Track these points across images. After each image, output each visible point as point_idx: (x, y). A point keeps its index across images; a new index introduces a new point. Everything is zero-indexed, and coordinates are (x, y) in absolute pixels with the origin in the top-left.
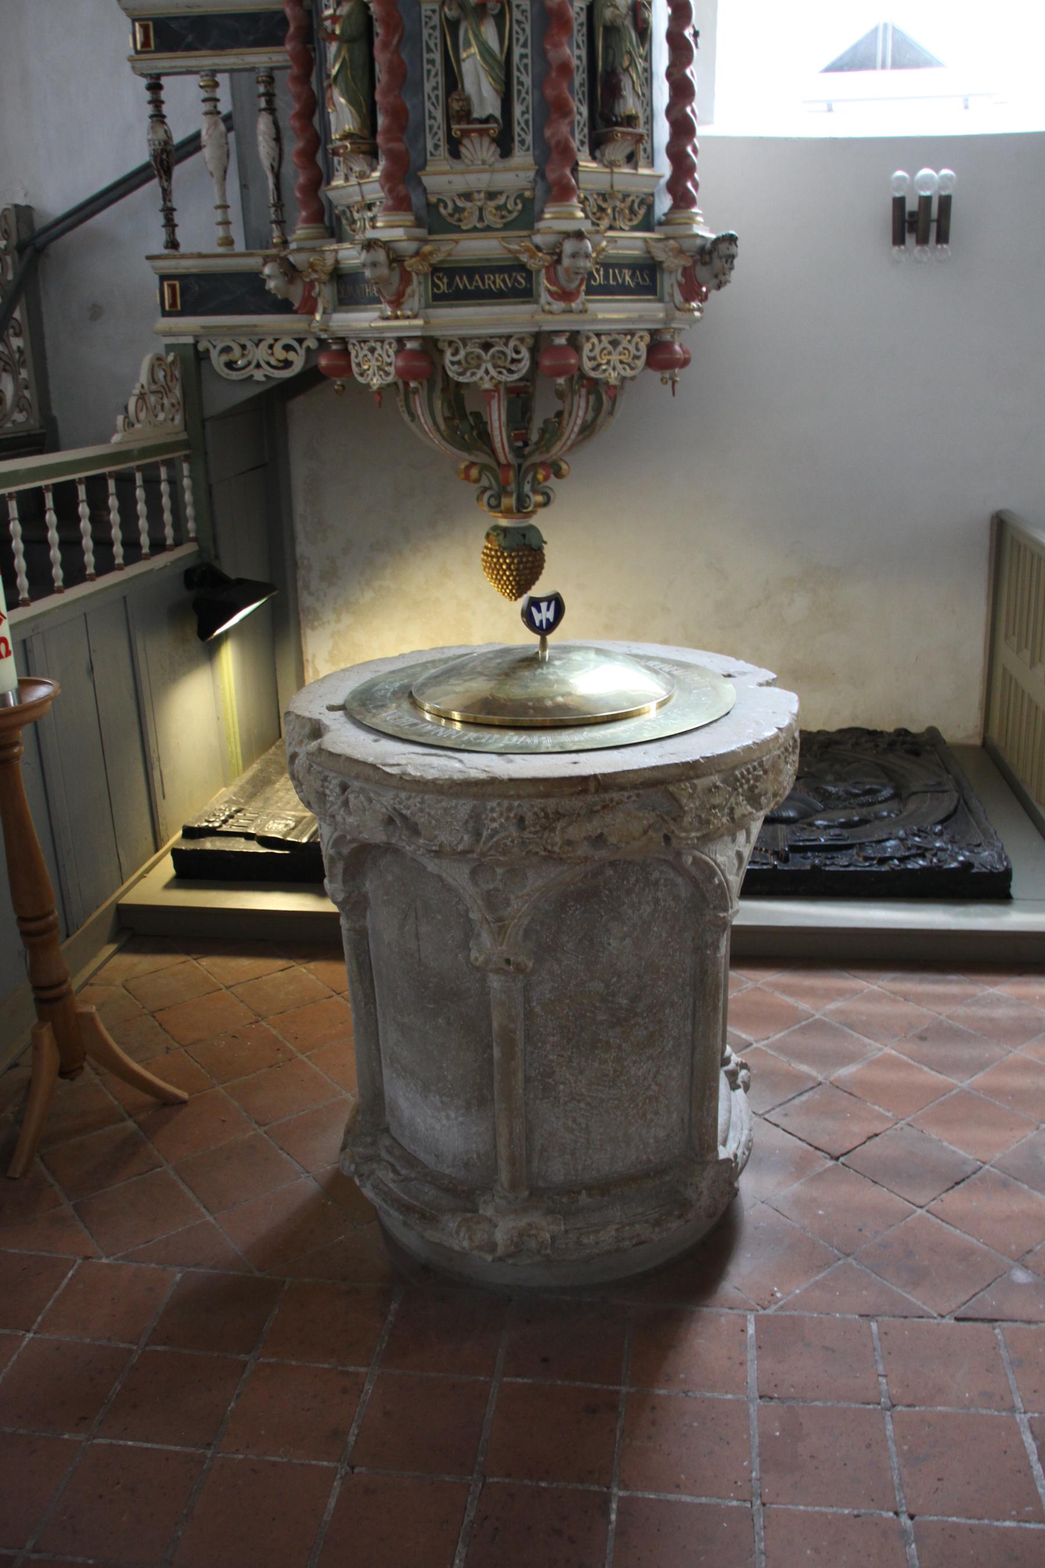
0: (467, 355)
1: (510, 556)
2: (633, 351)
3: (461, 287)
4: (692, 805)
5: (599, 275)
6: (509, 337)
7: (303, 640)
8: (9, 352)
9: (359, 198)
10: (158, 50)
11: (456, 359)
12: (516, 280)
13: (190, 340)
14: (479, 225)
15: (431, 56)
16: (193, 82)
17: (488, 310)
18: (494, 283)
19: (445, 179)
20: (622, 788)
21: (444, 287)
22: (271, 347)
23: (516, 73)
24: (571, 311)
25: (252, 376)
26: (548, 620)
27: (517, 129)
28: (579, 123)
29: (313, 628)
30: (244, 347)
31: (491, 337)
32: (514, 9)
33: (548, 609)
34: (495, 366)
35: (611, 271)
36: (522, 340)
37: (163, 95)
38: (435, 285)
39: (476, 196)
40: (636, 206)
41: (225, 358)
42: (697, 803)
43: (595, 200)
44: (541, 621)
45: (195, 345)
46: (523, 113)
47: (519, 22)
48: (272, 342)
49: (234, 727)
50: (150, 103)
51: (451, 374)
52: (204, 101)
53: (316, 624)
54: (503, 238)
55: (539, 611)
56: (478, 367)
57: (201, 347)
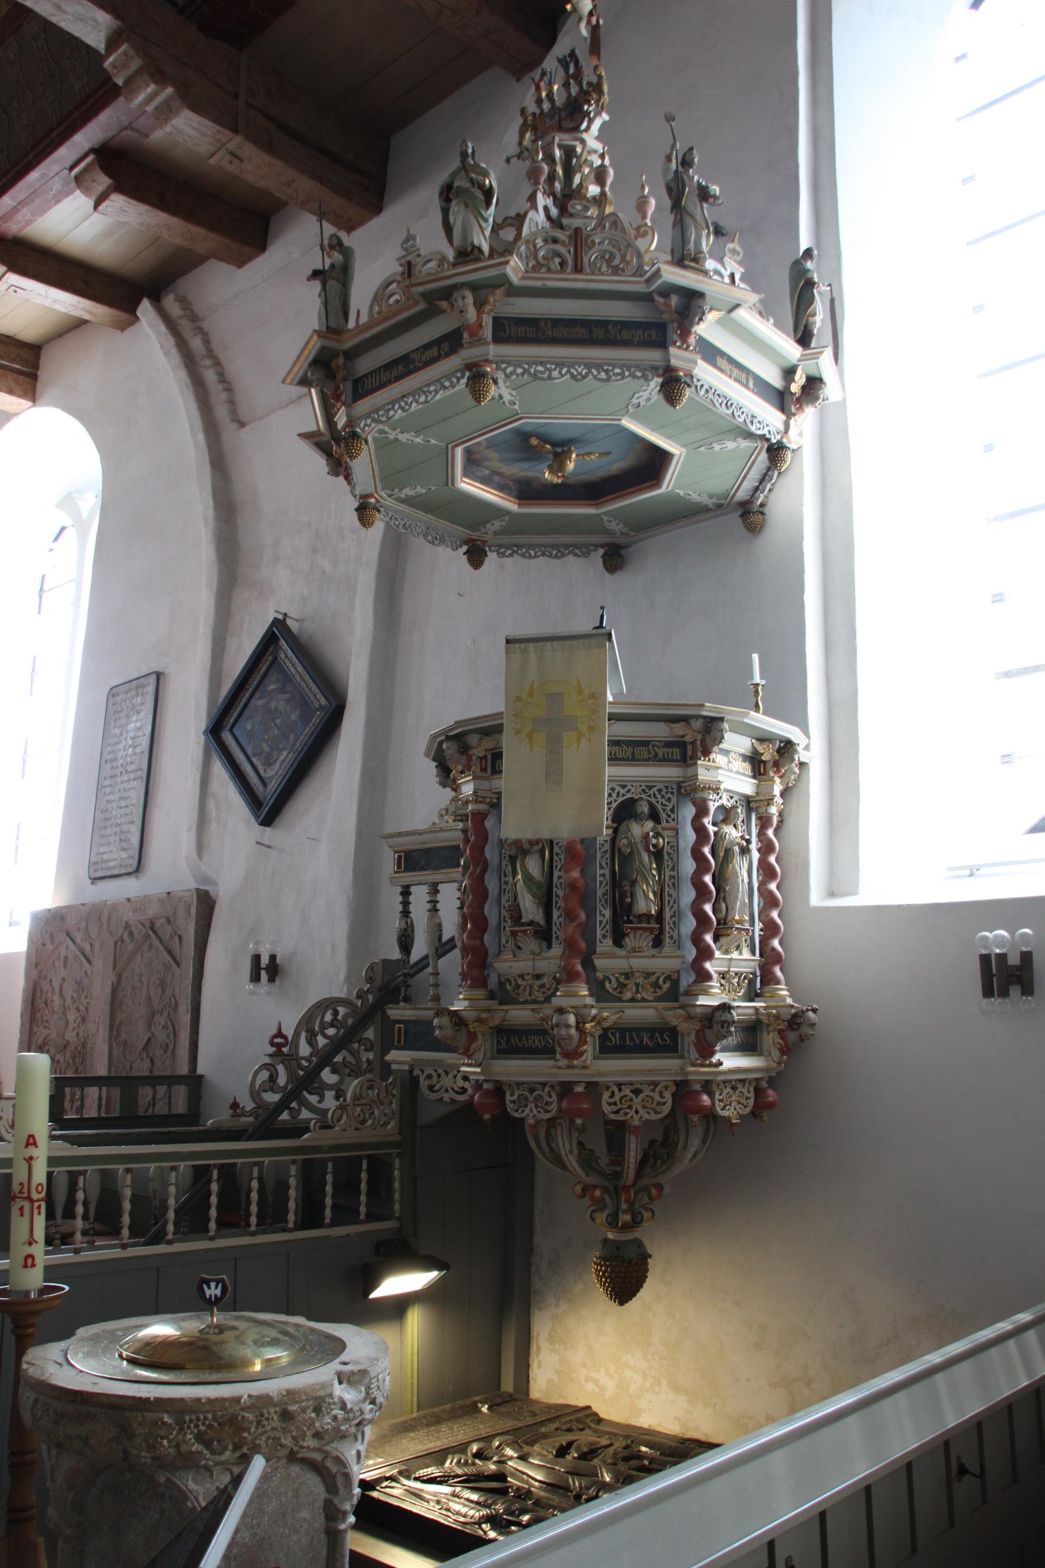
0: (519, 1096)
1: (605, 1265)
2: (746, 1093)
3: (514, 1044)
4: (141, 1431)
5: (615, 1038)
6: (544, 1084)
7: (532, 1317)
8: (357, 1063)
9: (558, 961)
10: (405, 871)
11: (513, 1098)
12: (547, 1041)
13: (406, 1067)
14: (529, 999)
15: (506, 879)
16: (425, 889)
17: (527, 1062)
18: (534, 1042)
19: (507, 964)
20: (95, 1405)
21: (504, 1044)
22: (455, 1077)
23: (555, 889)
24: (574, 1067)
25: (442, 1098)
26: (216, 1296)
27: (554, 929)
28: (601, 922)
29: (540, 1309)
30: (439, 1075)
31: (535, 1083)
32: (555, 846)
33: (216, 1288)
34: (536, 1106)
35: (628, 1034)
36: (553, 1087)
37: (411, 898)
38: (499, 1042)
39: (526, 977)
40: (661, 981)
41: (427, 1082)
42: (146, 1431)
43: (617, 979)
44: (211, 1295)
45: (411, 1071)
46: (559, 917)
47: (557, 854)
48: (456, 1073)
49: (412, 1378)
50: (401, 903)
51: (509, 1110)
52: (428, 902)
53: (542, 1305)
54: (533, 1010)
55: (209, 1288)
56: (526, 1106)
57: (415, 1073)
